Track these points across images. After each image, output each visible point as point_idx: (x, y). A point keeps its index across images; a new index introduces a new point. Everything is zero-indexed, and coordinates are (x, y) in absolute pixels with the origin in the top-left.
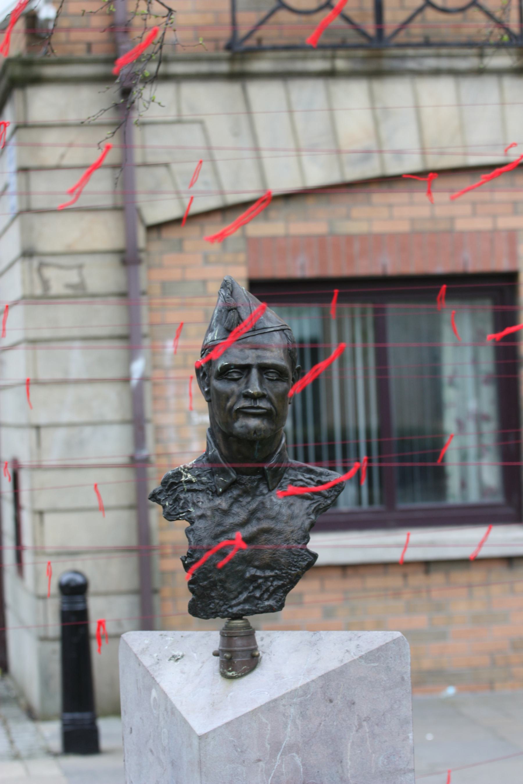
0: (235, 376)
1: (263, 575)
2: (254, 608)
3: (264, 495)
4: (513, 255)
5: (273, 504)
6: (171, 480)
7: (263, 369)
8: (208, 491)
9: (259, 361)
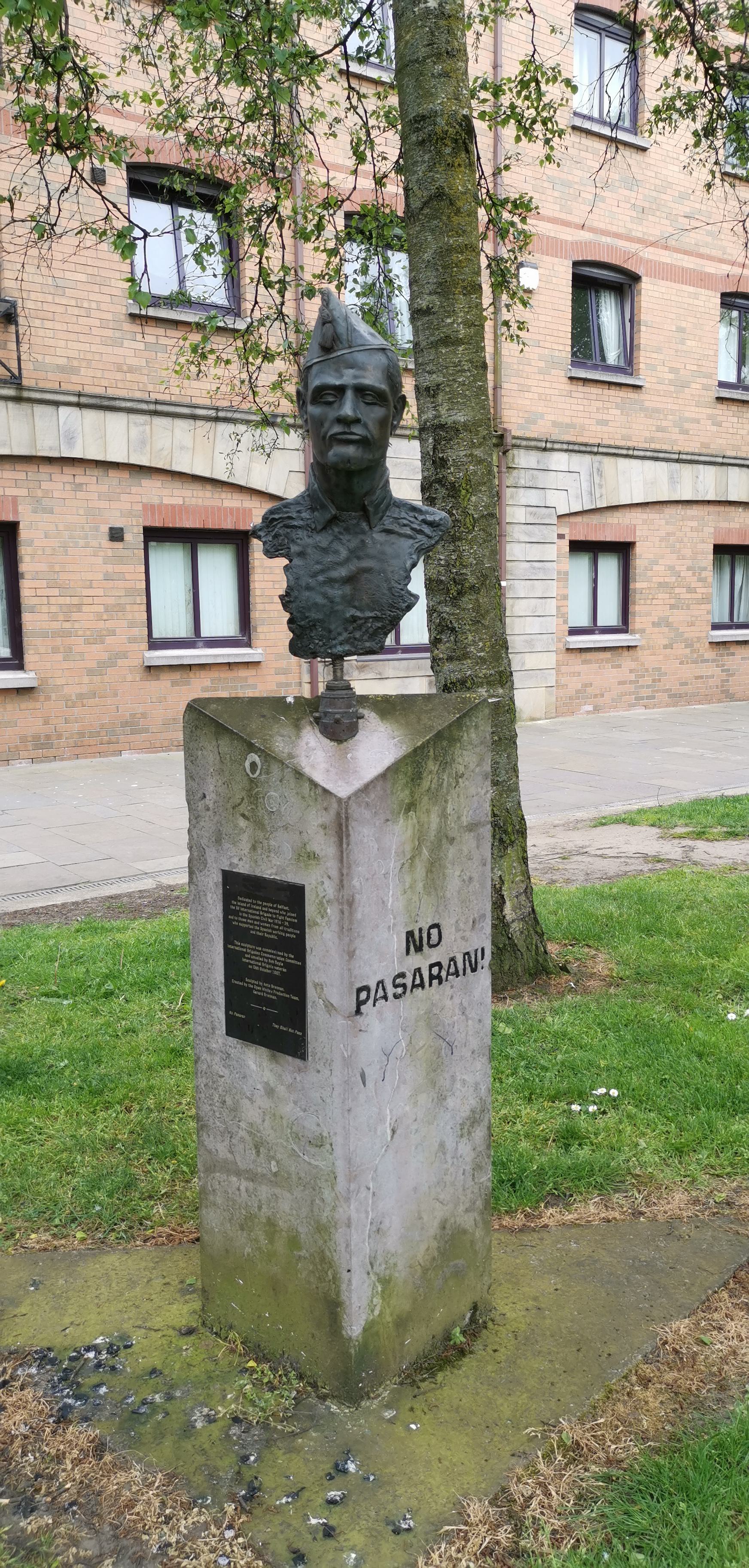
0: (331, 399)
3: (363, 532)
4: (16, 511)
5: (374, 542)
7: (361, 391)
9: (355, 382)
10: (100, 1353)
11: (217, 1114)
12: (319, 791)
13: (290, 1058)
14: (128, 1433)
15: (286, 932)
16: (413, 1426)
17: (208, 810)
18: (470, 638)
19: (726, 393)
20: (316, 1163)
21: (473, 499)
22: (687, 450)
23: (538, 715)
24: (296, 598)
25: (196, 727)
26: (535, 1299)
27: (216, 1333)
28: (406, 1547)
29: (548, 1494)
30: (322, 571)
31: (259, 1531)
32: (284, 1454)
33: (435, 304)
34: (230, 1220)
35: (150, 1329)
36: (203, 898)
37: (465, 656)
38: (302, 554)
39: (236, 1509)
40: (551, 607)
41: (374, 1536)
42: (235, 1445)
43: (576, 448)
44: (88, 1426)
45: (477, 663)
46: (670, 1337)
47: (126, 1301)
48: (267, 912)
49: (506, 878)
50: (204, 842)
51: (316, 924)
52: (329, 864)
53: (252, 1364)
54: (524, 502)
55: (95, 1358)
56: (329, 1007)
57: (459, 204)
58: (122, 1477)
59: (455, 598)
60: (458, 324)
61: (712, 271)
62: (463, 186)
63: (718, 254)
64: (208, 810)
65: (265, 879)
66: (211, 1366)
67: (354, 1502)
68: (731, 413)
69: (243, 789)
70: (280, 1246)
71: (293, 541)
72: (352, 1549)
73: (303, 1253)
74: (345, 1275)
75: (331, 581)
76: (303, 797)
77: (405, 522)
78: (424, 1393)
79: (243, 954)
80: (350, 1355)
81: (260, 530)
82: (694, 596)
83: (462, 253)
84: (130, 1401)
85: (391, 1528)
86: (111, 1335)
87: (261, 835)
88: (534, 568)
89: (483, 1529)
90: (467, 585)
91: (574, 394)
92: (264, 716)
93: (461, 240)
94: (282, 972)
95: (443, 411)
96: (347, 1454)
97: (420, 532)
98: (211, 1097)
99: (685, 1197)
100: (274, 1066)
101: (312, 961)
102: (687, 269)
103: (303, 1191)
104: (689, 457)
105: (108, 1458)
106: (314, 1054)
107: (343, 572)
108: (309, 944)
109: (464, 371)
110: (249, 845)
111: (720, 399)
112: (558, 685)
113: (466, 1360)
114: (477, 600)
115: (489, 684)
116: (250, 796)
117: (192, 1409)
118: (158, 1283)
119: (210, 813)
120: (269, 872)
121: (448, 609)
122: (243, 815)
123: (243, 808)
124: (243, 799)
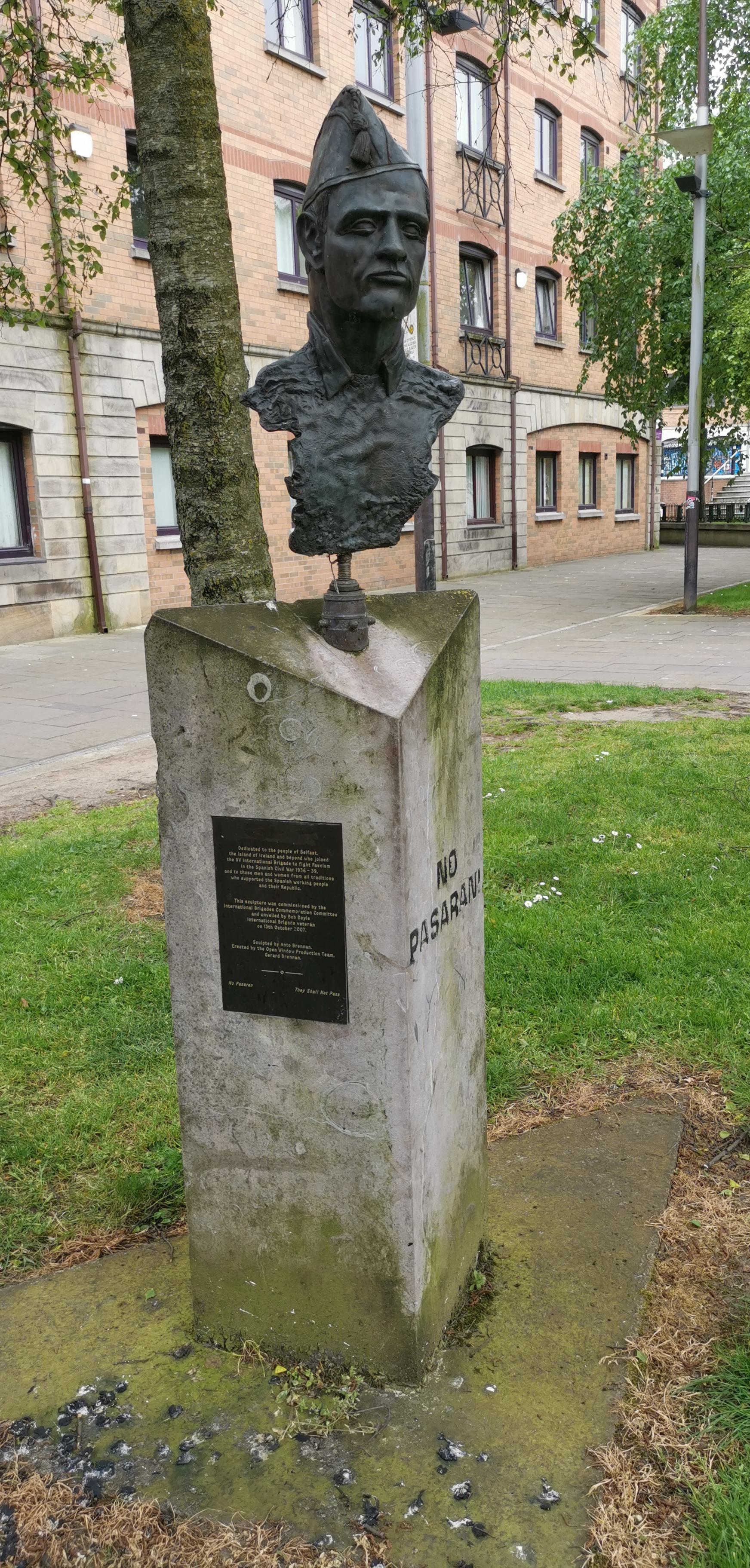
1: (379, 501)
2: (366, 542)
3: (380, 400)
6: (268, 379)
9: (400, 208)
10: (94, 1406)
11: (213, 1102)
12: (362, 712)
13: (322, 1025)
14: (187, 1491)
15: (313, 881)
16: (490, 1389)
17: (189, 746)
18: (233, 535)
19: (286, 286)
20: (362, 1136)
21: (228, 377)
22: (255, 342)
23: (134, 621)
24: (308, 480)
25: (167, 646)
26: (521, 1222)
27: (219, 1346)
28: (565, 1520)
29: (661, 1420)
30: (336, 447)
31: (407, 1556)
32: (378, 1459)
33: (173, 147)
34: (235, 1219)
35: (137, 1362)
36: (183, 853)
37: (229, 555)
38: (312, 426)
39: (369, 1538)
40: (138, 505)
41: (527, 1520)
42: (317, 1467)
43: (148, 335)
44: (135, 1497)
45: (242, 563)
46: (668, 1229)
47: (86, 1337)
48: (285, 860)
50: (183, 785)
51: (358, 867)
52: (377, 797)
53: (280, 1369)
54: (99, 392)
55: (91, 1413)
56: (380, 960)
57: (195, 30)
58: (212, 1545)
59: (214, 491)
60: (201, 173)
61: (264, 155)
62: (197, 9)
63: (268, 137)
64: (189, 746)
66: (234, 1385)
67: (484, 1489)
68: (292, 307)
69: (245, 717)
70: (311, 1234)
71: (299, 409)
72: (514, 1541)
73: (345, 1236)
74: (404, 1249)
77: (422, 388)
78: (478, 1350)
80: (413, 1332)
81: (254, 395)
82: (273, 493)
83: (200, 89)
84: (165, 1452)
85: (537, 1505)
86: (93, 1382)
87: (273, 770)
88: (117, 464)
89: (626, 1475)
90: (226, 475)
91: (141, 277)
92: (253, 628)
93: (198, 73)
94: (308, 928)
95: (189, 274)
96: (443, 1439)
97: (437, 400)
98: (203, 1084)
99: (589, 1086)
100: (298, 1035)
101: (354, 912)
102: (240, 150)
103: (344, 1169)
104: (258, 350)
105: (183, 1527)
106: (358, 1016)
107: (356, 449)
110: (256, 784)
111: (282, 291)
112: (152, 589)
113: (496, 1303)
114: (238, 492)
116: (255, 725)
117: (244, 1440)
118: (110, 1305)
119: (193, 749)
120: (287, 813)
121: (205, 503)
122: (245, 749)
123: (244, 741)
124: (244, 730)
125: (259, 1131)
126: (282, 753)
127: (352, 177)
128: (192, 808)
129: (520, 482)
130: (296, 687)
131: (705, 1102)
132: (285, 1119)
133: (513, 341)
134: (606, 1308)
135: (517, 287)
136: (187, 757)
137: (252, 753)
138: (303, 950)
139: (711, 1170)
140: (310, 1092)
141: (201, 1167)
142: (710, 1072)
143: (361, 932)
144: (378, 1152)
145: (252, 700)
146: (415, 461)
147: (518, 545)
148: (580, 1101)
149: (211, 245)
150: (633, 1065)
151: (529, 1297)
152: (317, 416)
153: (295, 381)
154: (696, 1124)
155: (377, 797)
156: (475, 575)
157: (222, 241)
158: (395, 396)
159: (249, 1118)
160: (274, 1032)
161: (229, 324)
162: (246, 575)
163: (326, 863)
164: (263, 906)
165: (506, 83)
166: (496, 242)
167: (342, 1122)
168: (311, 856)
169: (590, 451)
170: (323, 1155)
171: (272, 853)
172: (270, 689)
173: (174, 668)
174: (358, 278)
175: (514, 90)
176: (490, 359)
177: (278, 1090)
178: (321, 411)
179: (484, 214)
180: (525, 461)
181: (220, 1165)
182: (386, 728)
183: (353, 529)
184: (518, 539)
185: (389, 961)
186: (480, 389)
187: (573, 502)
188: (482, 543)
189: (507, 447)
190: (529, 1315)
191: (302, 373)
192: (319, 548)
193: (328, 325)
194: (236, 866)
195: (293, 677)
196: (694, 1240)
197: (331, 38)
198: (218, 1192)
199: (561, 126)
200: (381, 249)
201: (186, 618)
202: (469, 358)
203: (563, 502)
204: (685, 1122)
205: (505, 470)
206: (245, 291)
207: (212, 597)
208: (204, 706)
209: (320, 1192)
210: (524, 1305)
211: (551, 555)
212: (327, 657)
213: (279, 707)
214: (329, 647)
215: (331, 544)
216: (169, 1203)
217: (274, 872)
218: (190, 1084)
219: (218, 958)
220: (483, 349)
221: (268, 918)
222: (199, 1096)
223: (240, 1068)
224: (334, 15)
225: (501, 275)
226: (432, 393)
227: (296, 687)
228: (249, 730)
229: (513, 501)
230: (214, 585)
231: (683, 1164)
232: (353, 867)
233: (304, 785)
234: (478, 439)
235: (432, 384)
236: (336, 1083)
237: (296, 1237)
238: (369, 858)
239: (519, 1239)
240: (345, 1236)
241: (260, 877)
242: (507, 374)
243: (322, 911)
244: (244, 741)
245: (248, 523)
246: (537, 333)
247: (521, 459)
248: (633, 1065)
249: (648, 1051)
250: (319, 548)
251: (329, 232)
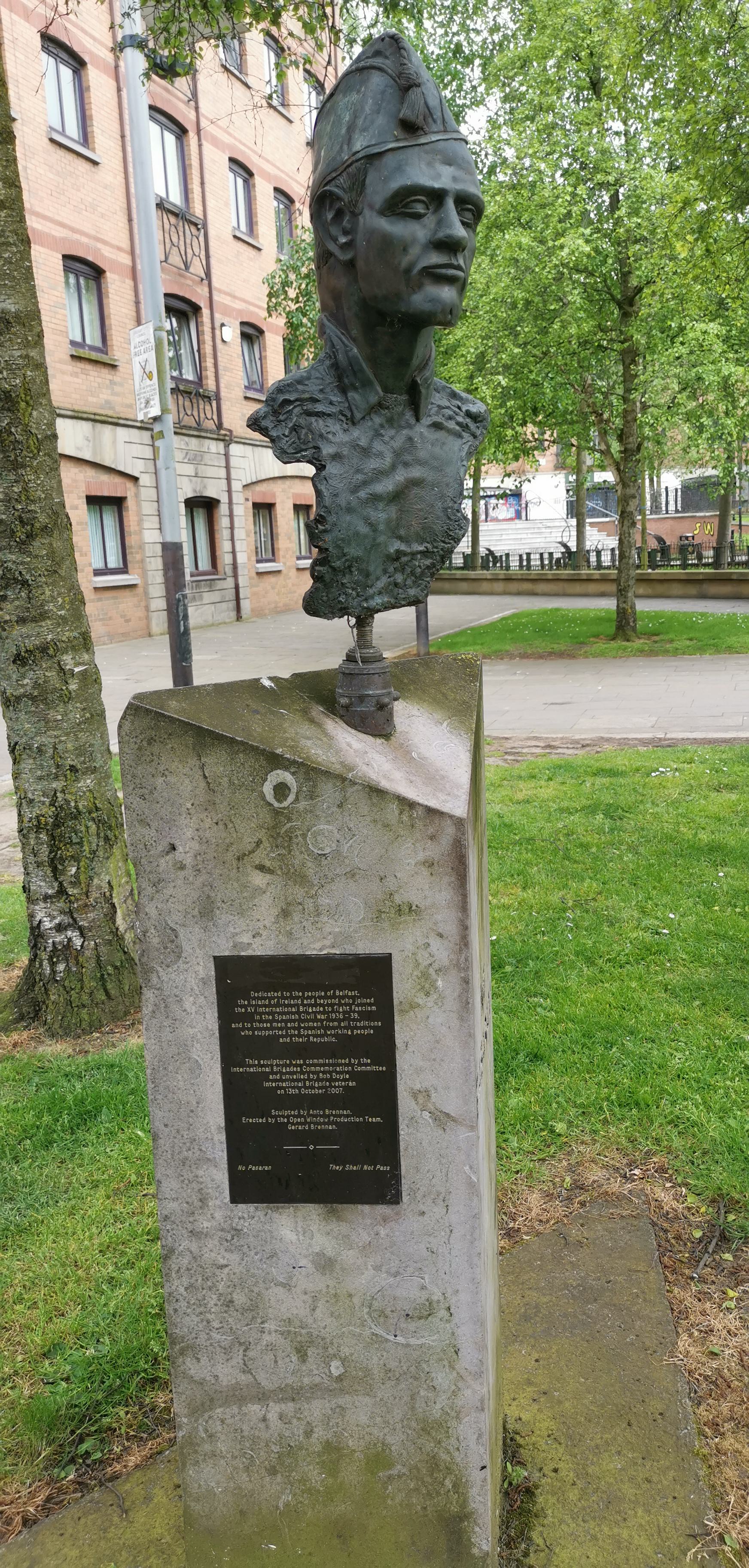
0: (420, 209)
1: (409, 550)
2: (393, 601)
3: (410, 426)
6: (281, 398)
8: (340, 417)
9: (459, 187)
13: (366, 1208)
15: (353, 1028)
17: (182, 867)
18: (48, 593)
20: (419, 1342)
21: (35, 413)
25: (151, 741)
26: (529, 1383)
30: (365, 483)
34: (247, 1469)
36: (174, 1007)
37: (43, 616)
38: (336, 457)
45: (59, 625)
48: (315, 1005)
49: (114, 883)
51: (413, 1006)
56: (442, 1119)
64: (182, 867)
65: (308, 958)
71: (321, 436)
73: (398, 1469)
75: (375, 498)
76: (386, 826)
77: (451, 413)
79: (265, 1076)
81: (265, 417)
87: (299, 892)
90: (37, 525)
92: (257, 712)
94: (346, 1088)
97: (465, 427)
98: (202, 1302)
106: (413, 1192)
107: (385, 486)
108: (400, 1038)
109: (9, 244)
110: (275, 911)
114: (51, 544)
115: (74, 648)
119: (188, 872)
120: (318, 945)
121: (14, 557)
122: (261, 868)
123: (259, 857)
124: (259, 843)
125: (280, 1354)
126: (311, 869)
127: (401, 144)
128: (187, 948)
129: (239, 534)
130: (330, 785)
131: (664, 1195)
132: (315, 1333)
133: (223, 394)
134: (665, 1482)
135: (223, 341)
136: (179, 882)
137: (270, 871)
138: (340, 1116)
139: (702, 1280)
140: (350, 1296)
141: (197, 1410)
142: (655, 1159)
143: (418, 1086)
144: (441, 1360)
145: (270, 805)
146: (449, 500)
147: (241, 596)
148: (533, 1214)
149: (11, 263)
150: (573, 1162)
151: (574, 1484)
152: (344, 444)
153: (315, 401)
154: (666, 1225)
155: (439, 917)
156: (201, 627)
157: (22, 259)
158: (426, 421)
159: (266, 1338)
160: (300, 1224)
161: (33, 353)
162: (64, 639)
163: (370, 1005)
164: (286, 1065)
165: (199, 140)
166: (199, 295)
167: (392, 1329)
168: (349, 997)
169: (303, 503)
170: (367, 1372)
171: (298, 998)
172: (294, 790)
173: (161, 768)
174: (408, 271)
175: (207, 147)
176: (202, 411)
177: (305, 1297)
178: (346, 438)
179: (187, 267)
180: (243, 512)
181: (226, 1403)
182: (450, 830)
183: (380, 584)
184: (241, 591)
185: (454, 1120)
186: (194, 441)
187: (290, 553)
188: (205, 595)
189: (224, 498)
190: (584, 1508)
191: (321, 391)
192: (341, 609)
193: (354, 332)
194: (248, 1017)
195: (327, 774)
196: (718, 1371)
197: (21, 80)
198: (223, 1437)
199: (254, 186)
200: (441, 235)
201: (173, 704)
202: (181, 409)
203: (281, 553)
204: (654, 1224)
205: (223, 522)
206: (48, 319)
207: (24, 664)
208: (203, 816)
209: (363, 1419)
210: (573, 1495)
211: (273, 606)
212: (356, 745)
213: (306, 811)
214: (353, 731)
215: (355, 604)
216: (93, 1429)
217: (300, 1021)
218: (183, 1304)
219: (223, 1137)
220: (194, 401)
221: (293, 1080)
222: (196, 1319)
223: (253, 1276)
224: (22, 57)
225: (207, 328)
226: (460, 419)
227: (330, 785)
228: (266, 844)
229: (234, 552)
230: (27, 651)
231: (671, 1278)
232: (407, 1008)
233: (341, 908)
234: (195, 491)
235: (459, 408)
236: (383, 1279)
237: (331, 1480)
238: (427, 994)
239: (536, 1407)
240: (398, 1469)
241: (281, 1029)
242: (220, 426)
243: (365, 1065)
244: (259, 857)
245: (63, 578)
246: (246, 387)
247: (239, 510)
248: (573, 1162)
249: (583, 1143)
250: (341, 609)
251: (367, 212)
